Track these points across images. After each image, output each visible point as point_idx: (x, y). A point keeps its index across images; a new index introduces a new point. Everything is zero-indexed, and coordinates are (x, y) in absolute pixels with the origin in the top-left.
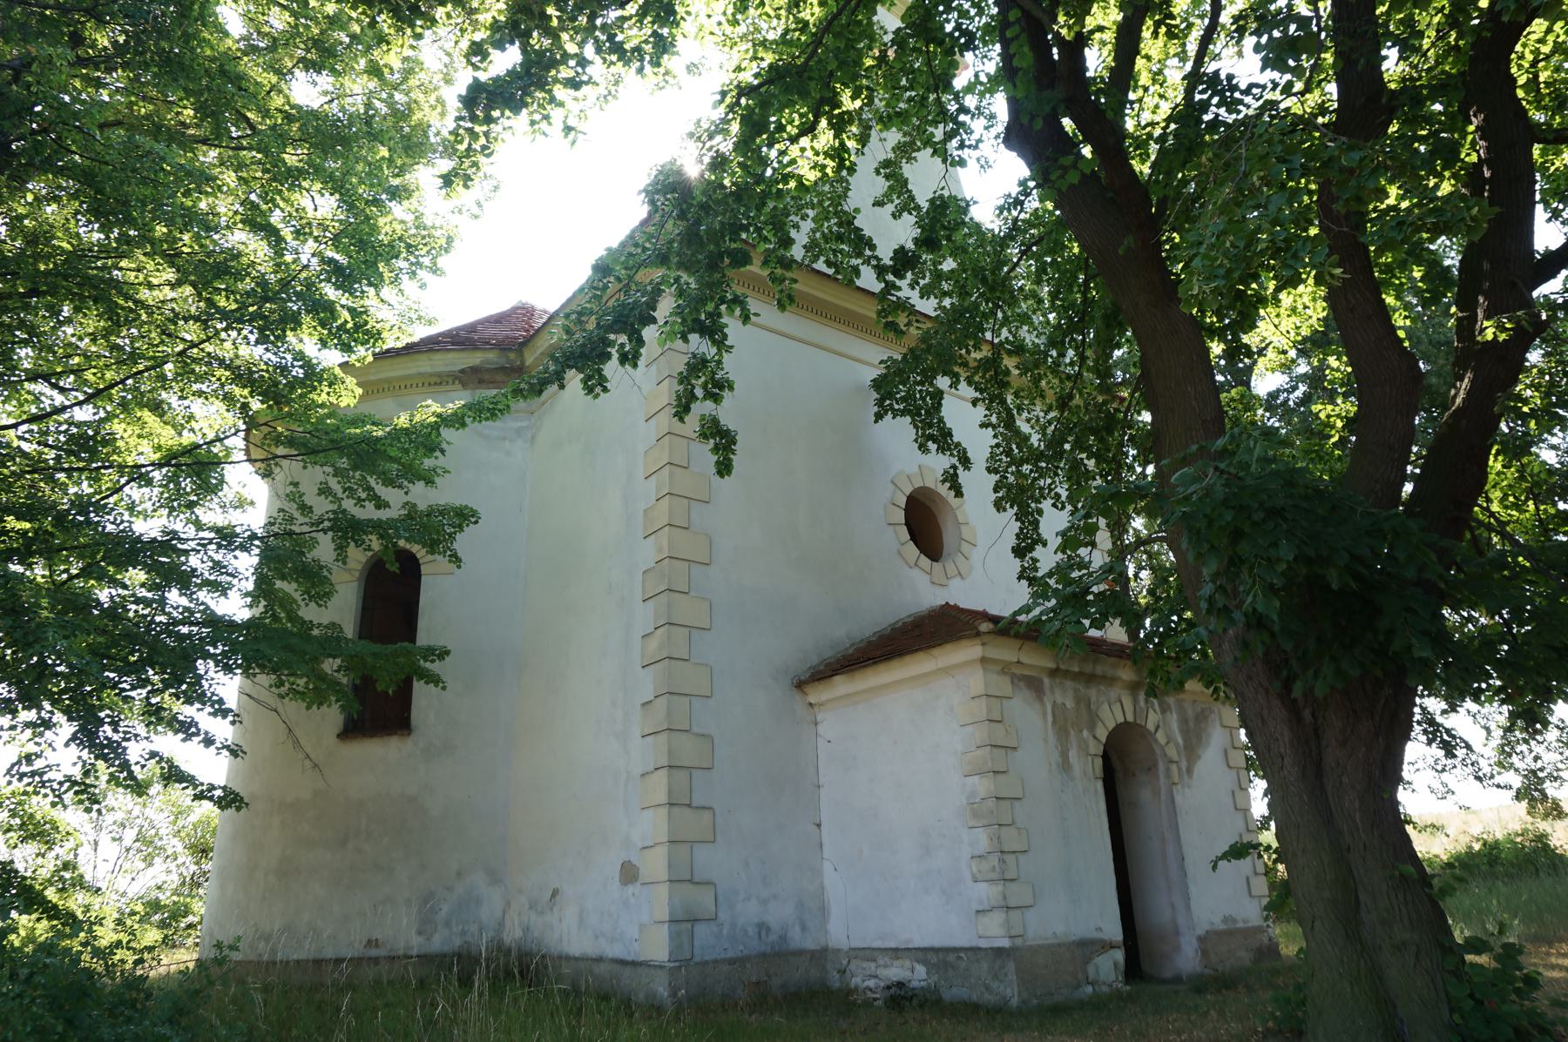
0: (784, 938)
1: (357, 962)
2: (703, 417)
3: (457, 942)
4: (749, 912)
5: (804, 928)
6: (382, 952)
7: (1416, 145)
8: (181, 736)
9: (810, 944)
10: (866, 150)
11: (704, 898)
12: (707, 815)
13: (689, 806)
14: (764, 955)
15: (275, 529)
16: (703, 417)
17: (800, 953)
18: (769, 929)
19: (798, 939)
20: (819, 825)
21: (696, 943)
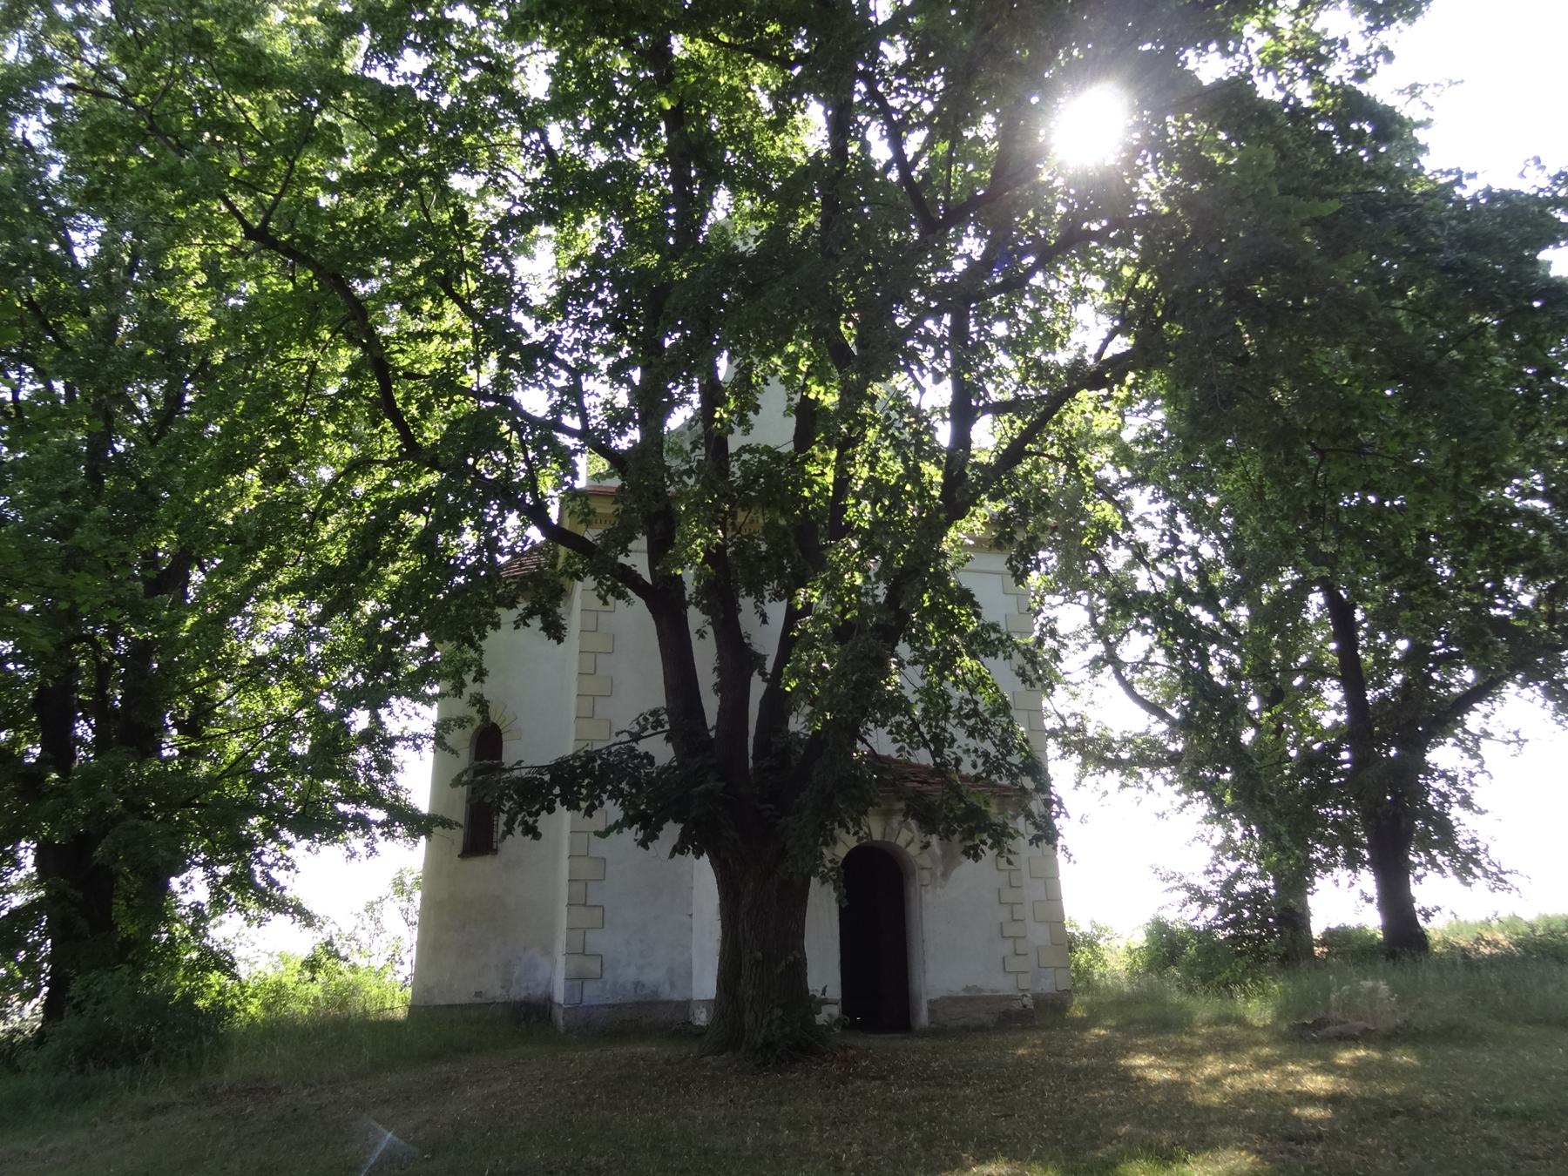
0: (655, 993)
1: (469, 1006)
2: (471, 695)
3: (523, 994)
4: (629, 975)
5: (672, 985)
6: (483, 1000)
7: (1085, 225)
8: (489, 631)
9: (677, 997)
10: (282, 884)
11: (593, 966)
12: (598, 912)
13: (585, 905)
14: (637, 1003)
15: (253, 909)
16: (471, 695)
17: (668, 1002)
18: (643, 986)
19: (667, 993)
20: (691, 916)
21: (585, 993)
